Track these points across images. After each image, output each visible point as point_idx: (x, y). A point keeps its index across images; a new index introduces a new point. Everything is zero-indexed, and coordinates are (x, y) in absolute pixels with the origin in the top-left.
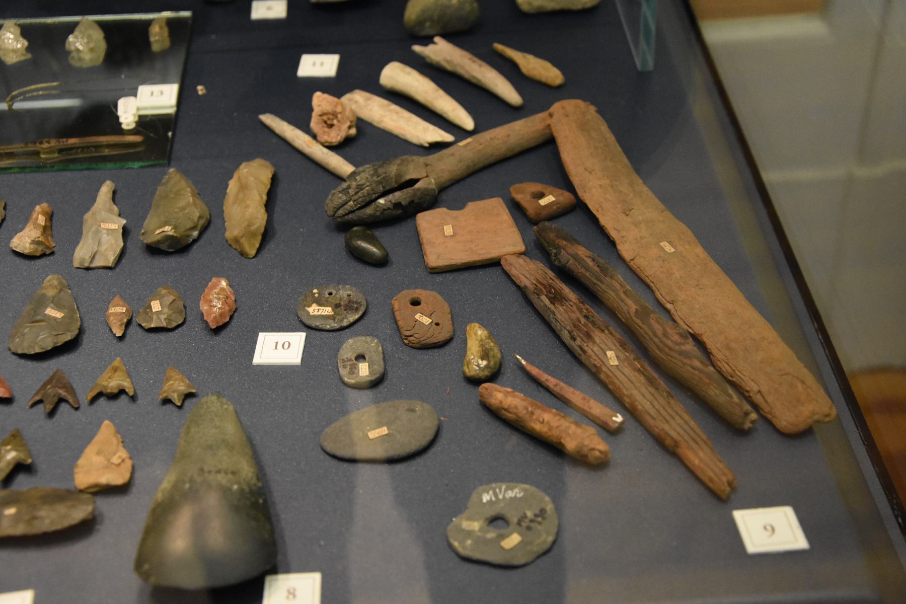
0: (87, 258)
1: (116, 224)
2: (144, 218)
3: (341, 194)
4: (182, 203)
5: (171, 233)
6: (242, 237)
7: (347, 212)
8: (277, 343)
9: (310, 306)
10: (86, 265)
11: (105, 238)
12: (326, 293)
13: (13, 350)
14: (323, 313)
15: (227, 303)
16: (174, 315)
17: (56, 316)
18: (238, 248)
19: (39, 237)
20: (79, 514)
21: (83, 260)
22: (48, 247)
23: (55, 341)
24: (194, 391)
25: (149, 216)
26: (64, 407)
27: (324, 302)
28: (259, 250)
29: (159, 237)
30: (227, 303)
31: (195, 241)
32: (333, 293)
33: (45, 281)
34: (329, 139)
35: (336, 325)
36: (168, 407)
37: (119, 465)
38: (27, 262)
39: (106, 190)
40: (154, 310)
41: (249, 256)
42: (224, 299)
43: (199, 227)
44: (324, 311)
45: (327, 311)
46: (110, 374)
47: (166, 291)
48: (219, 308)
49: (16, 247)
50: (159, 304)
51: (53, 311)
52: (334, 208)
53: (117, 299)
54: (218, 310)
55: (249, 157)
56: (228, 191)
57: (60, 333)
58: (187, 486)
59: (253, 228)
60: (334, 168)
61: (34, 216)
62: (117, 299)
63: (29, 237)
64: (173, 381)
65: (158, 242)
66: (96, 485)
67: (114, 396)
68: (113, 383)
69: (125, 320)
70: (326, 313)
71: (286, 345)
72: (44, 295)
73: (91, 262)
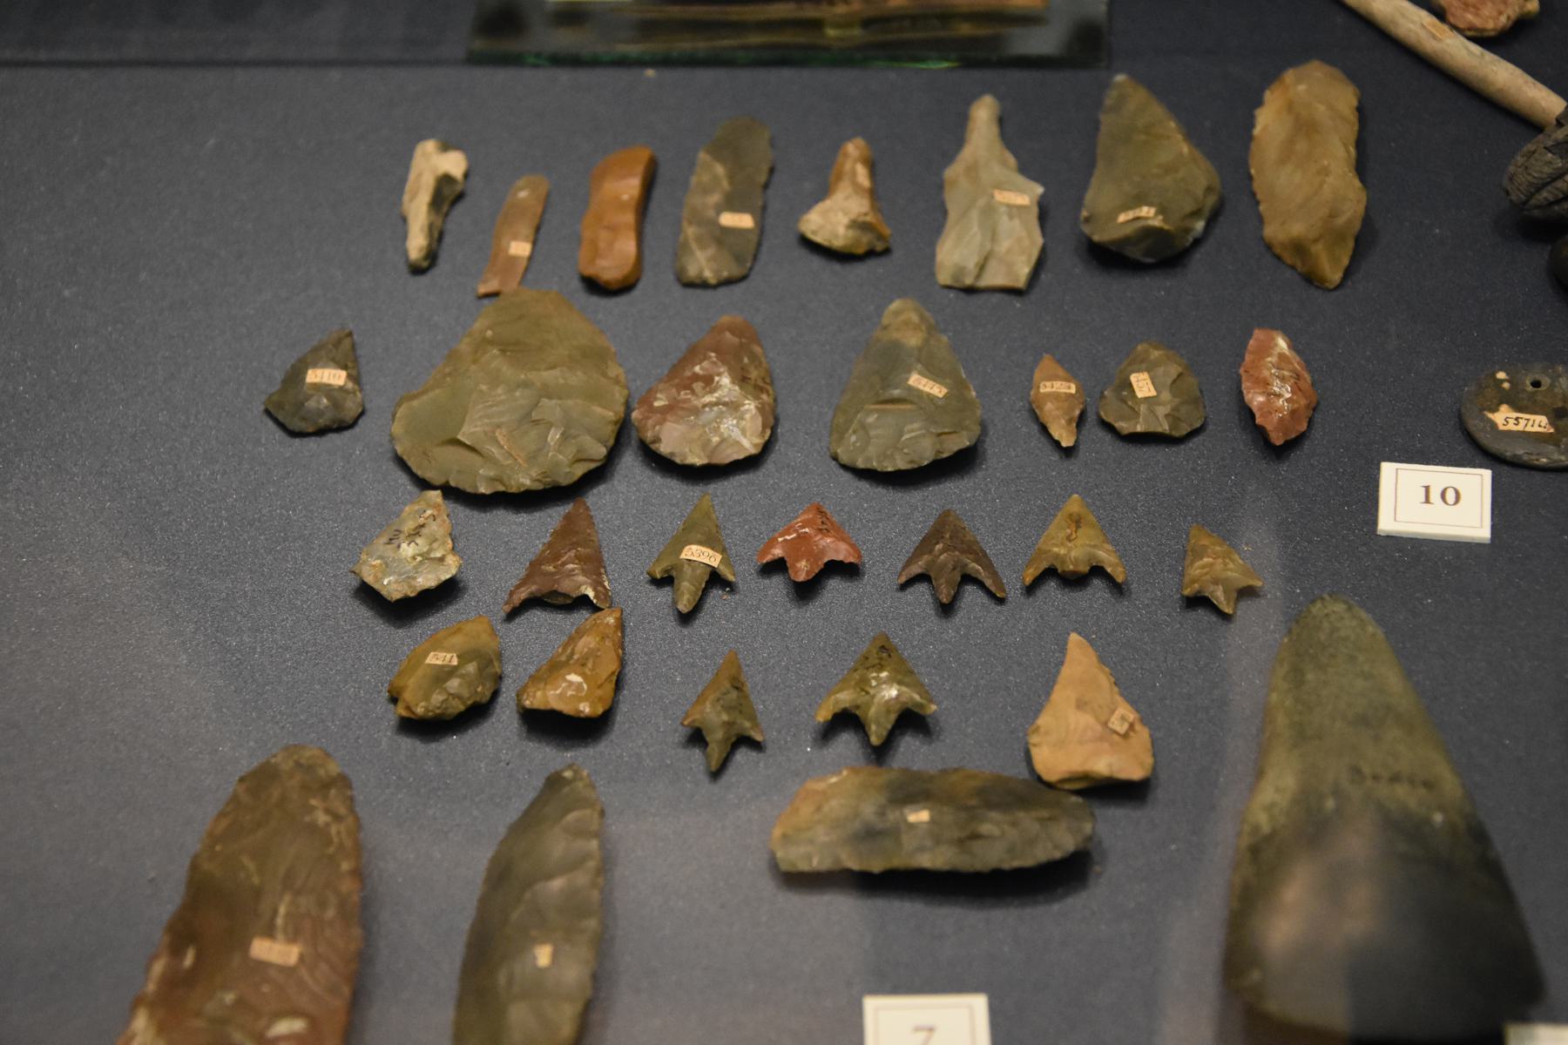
0: (971, 264)
1: (1023, 195)
2: (1084, 186)
3: (1550, 155)
4: (1164, 157)
5: (1157, 222)
6: (1316, 241)
7: (1561, 196)
8: (1427, 489)
9: (1495, 410)
10: (968, 281)
11: (1004, 223)
12: (1528, 383)
13: (844, 459)
14: (1529, 429)
15: (1300, 390)
16: (1184, 410)
17: (932, 392)
18: (1299, 264)
19: (866, 214)
20: (1058, 841)
21: (960, 271)
22: (881, 237)
23: (938, 447)
24: (1259, 584)
25: (1094, 181)
26: (971, 594)
27: (1525, 402)
28: (1348, 273)
29: (1128, 230)
30: (1300, 390)
31: (1197, 242)
32: (1543, 383)
33: (886, 313)
34: (1477, 22)
35: (1563, 458)
36: (1202, 614)
37: (1125, 736)
38: (837, 267)
39: (983, 113)
40: (1140, 395)
41: (1327, 284)
42: (1292, 381)
43: (1207, 212)
44: (1531, 423)
45: (1538, 423)
46: (1069, 531)
47: (1161, 352)
48: (1288, 400)
49: (814, 232)
50: (1150, 383)
51: (924, 380)
52: (1531, 184)
53: (1047, 363)
54: (1286, 404)
55: (1297, 55)
56: (1257, 131)
57: (946, 430)
58: (1330, 804)
59: (1341, 221)
60: (1501, 90)
61: (848, 167)
62: (1047, 363)
63: (845, 213)
64: (1209, 557)
65: (1126, 241)
66: (1085, 777)
67: (1074, 581)
68: (1075, 550)
69: (1077, 412)
70: (1536, 429)
71: (1450, 496)
72: (896, 346)
73: (978, 276)
